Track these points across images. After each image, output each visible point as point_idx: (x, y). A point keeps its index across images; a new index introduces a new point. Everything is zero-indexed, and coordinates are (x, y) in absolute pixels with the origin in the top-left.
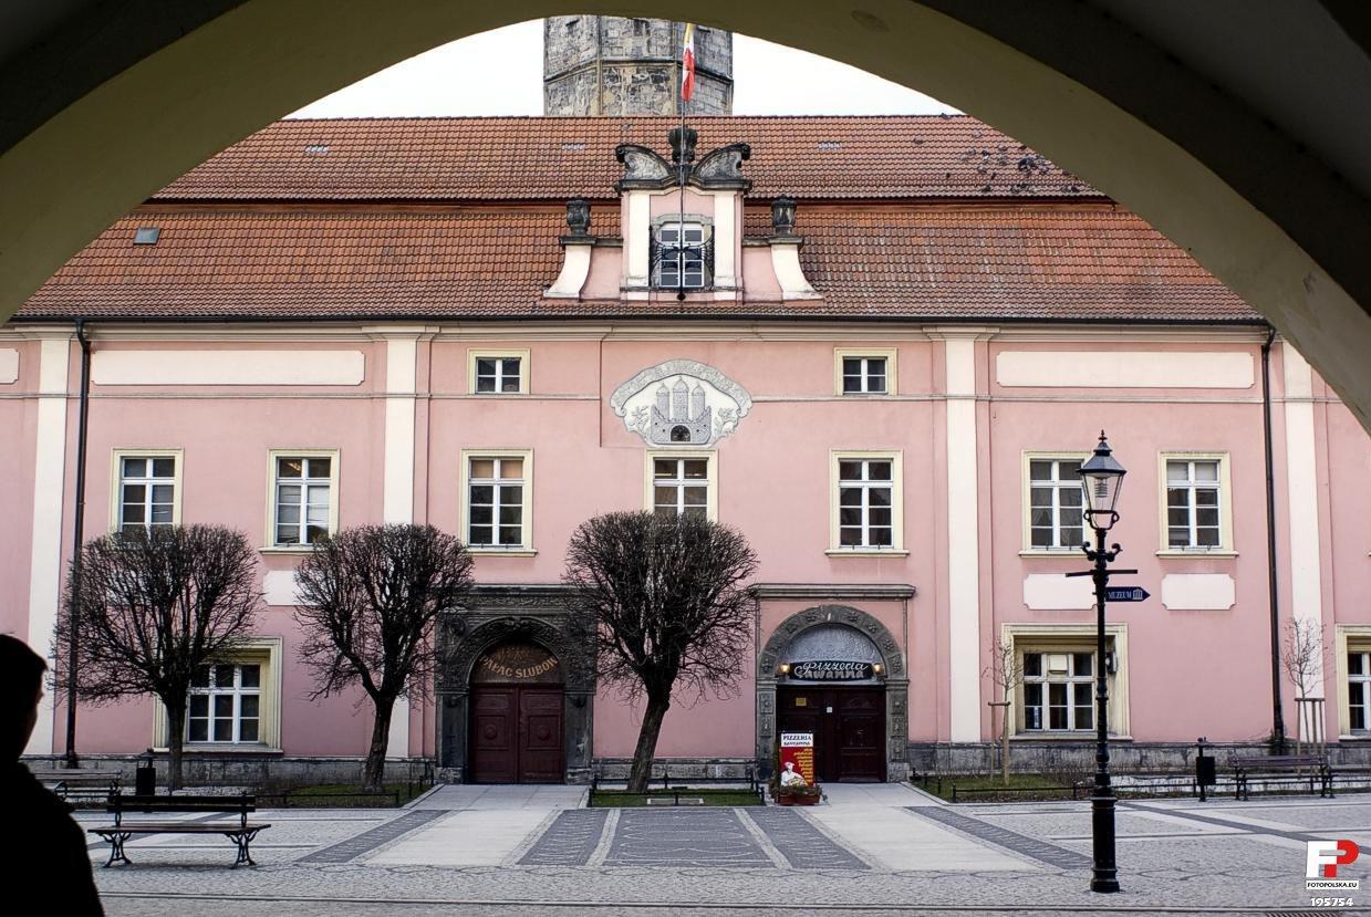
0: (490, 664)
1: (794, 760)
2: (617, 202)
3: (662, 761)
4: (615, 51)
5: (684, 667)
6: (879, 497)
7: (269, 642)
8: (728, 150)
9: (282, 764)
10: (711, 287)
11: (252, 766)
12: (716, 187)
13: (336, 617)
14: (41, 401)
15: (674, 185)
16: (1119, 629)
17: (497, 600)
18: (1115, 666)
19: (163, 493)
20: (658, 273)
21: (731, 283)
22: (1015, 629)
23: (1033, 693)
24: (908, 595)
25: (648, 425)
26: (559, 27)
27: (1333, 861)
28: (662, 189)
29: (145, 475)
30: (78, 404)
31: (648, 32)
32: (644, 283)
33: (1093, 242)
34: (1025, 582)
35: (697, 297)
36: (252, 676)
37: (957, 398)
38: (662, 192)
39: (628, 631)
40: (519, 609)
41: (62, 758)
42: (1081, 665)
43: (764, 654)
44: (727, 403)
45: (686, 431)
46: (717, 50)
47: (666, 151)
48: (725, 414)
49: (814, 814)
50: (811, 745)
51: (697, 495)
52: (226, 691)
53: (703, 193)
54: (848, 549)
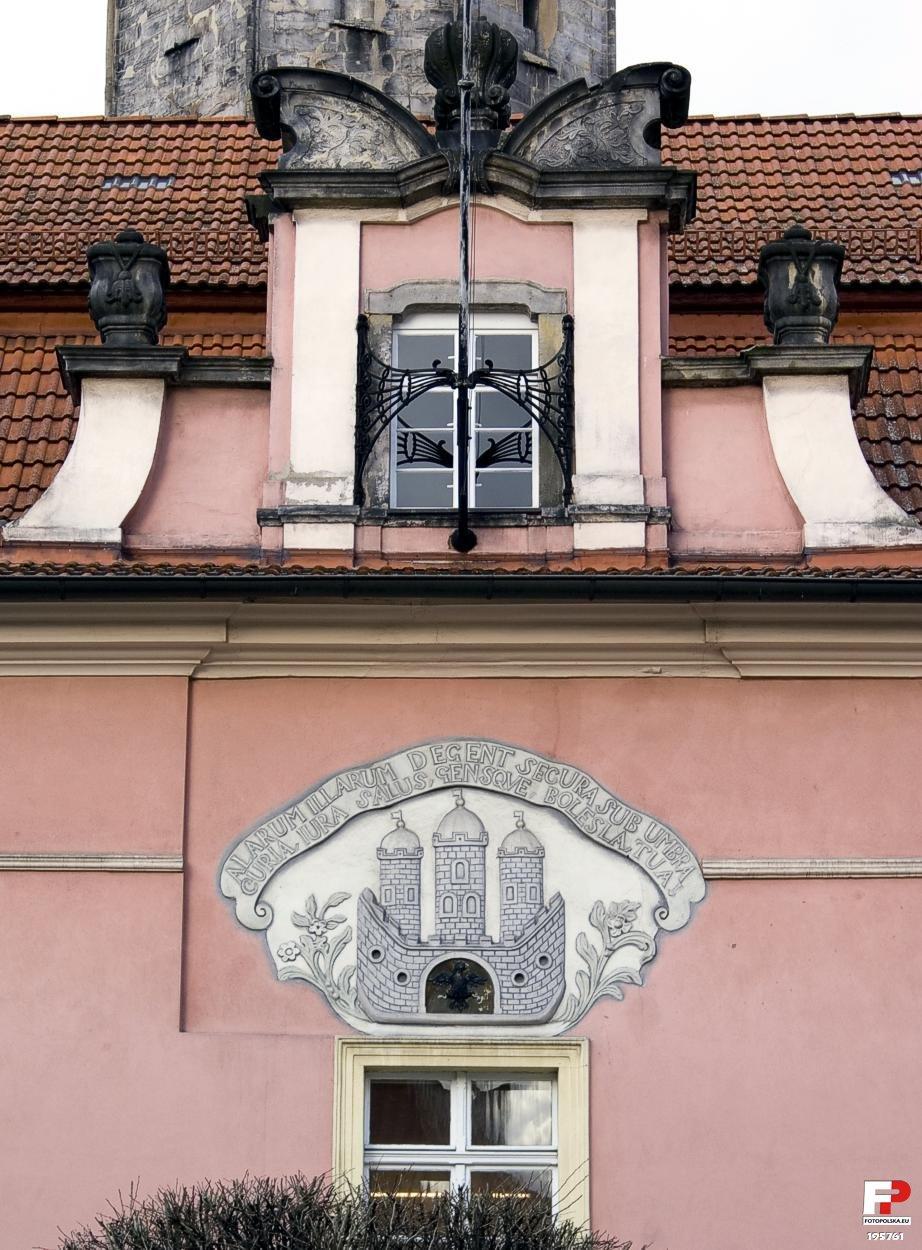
10: (563, 509)
21: (631, 495)
25: (349, 957)
27: (887, 1199)
28: (402, 203)
31: (386, 62)
32: (341, 494)
44: (618, 883)
45: (479, 977)
48: (615, 922)
53: (535, 216)
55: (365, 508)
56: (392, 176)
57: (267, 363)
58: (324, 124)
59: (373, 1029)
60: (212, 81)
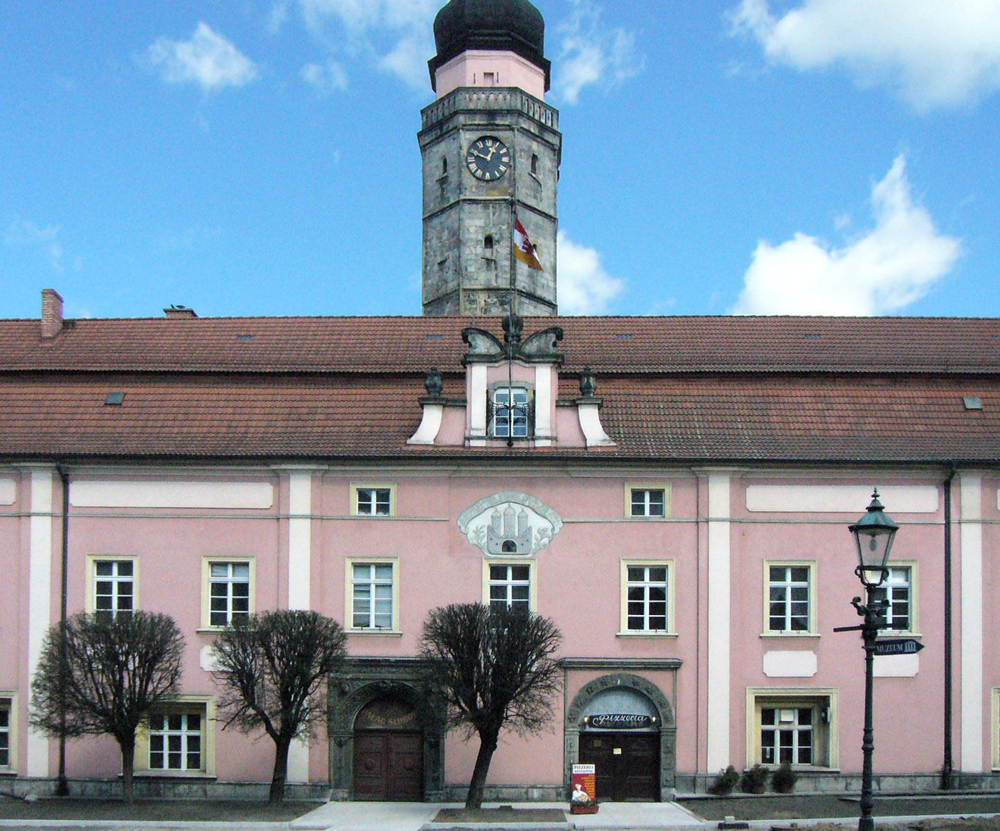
0: (370, 715)
1: (582, 783)
2: (462, 377)
3: (495, 786)
4: (473, 282)
5: (507, 718)
6: (658, 594)
7: (206, 698)
8: (546, 332)
9: (216, 786)
10: (533, 438)
11: (195, 787)
12: (537, 360)
13: (243, 678)
14: (33, 518)
15: (506, 359)
16: (833, 691)
17: (374, 669)
18: (829, 718)
19: (125, 588)
20: (494, 425)
21: (548, 434)
22: (756, 691)
23: (767, 738)
24: (674, 667)
25: (485, 540)
26: (433, 265)
28: (496, 362)
29: (111, 574)
30: (60, 521)
31: (496, 268)
32: (483, 433)
33: (820, 406)
35: (523, 444)
36: (195, 723)
37: (717, 520)
38: (496, 365)
39: (466, 688)
40: (388, 675)
41: (55, 780)
42: (804, 717)
43: (571, 711)
44: (544, 523)
45: (513, 544)
46: (545, 282)
47: (500, 334)
48: (542, 532)
50: (594, 772)
51: (522, 592)
52: (175, 733)
53: (527, 365)
54: (633, 632)
55: (488, 436)
56: (494, 356)
57: (465, 401)
58: (478, 342)
59: (490, 555)
60: (451, 272)
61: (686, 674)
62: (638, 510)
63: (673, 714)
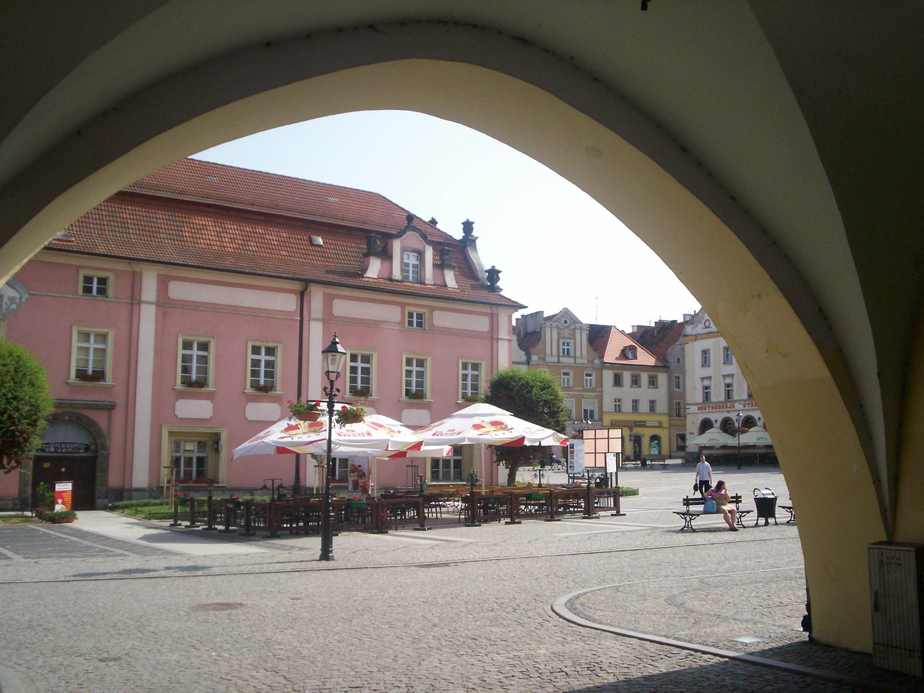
1: (62, 498)
16: (224, 429)
24: (111, 408)
34: (403, 412)
48: (12, 300)
49: (75, 524)
50: (71, 489)
61: (118, 415)
62: (88, 290)
63: (108, 443)
